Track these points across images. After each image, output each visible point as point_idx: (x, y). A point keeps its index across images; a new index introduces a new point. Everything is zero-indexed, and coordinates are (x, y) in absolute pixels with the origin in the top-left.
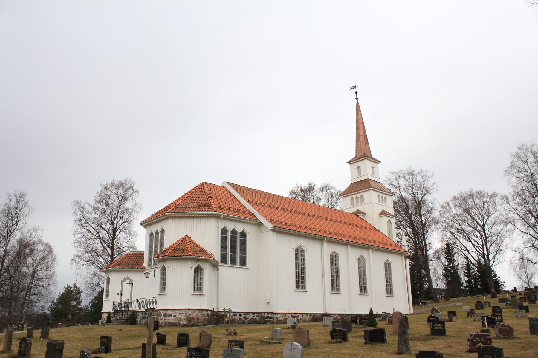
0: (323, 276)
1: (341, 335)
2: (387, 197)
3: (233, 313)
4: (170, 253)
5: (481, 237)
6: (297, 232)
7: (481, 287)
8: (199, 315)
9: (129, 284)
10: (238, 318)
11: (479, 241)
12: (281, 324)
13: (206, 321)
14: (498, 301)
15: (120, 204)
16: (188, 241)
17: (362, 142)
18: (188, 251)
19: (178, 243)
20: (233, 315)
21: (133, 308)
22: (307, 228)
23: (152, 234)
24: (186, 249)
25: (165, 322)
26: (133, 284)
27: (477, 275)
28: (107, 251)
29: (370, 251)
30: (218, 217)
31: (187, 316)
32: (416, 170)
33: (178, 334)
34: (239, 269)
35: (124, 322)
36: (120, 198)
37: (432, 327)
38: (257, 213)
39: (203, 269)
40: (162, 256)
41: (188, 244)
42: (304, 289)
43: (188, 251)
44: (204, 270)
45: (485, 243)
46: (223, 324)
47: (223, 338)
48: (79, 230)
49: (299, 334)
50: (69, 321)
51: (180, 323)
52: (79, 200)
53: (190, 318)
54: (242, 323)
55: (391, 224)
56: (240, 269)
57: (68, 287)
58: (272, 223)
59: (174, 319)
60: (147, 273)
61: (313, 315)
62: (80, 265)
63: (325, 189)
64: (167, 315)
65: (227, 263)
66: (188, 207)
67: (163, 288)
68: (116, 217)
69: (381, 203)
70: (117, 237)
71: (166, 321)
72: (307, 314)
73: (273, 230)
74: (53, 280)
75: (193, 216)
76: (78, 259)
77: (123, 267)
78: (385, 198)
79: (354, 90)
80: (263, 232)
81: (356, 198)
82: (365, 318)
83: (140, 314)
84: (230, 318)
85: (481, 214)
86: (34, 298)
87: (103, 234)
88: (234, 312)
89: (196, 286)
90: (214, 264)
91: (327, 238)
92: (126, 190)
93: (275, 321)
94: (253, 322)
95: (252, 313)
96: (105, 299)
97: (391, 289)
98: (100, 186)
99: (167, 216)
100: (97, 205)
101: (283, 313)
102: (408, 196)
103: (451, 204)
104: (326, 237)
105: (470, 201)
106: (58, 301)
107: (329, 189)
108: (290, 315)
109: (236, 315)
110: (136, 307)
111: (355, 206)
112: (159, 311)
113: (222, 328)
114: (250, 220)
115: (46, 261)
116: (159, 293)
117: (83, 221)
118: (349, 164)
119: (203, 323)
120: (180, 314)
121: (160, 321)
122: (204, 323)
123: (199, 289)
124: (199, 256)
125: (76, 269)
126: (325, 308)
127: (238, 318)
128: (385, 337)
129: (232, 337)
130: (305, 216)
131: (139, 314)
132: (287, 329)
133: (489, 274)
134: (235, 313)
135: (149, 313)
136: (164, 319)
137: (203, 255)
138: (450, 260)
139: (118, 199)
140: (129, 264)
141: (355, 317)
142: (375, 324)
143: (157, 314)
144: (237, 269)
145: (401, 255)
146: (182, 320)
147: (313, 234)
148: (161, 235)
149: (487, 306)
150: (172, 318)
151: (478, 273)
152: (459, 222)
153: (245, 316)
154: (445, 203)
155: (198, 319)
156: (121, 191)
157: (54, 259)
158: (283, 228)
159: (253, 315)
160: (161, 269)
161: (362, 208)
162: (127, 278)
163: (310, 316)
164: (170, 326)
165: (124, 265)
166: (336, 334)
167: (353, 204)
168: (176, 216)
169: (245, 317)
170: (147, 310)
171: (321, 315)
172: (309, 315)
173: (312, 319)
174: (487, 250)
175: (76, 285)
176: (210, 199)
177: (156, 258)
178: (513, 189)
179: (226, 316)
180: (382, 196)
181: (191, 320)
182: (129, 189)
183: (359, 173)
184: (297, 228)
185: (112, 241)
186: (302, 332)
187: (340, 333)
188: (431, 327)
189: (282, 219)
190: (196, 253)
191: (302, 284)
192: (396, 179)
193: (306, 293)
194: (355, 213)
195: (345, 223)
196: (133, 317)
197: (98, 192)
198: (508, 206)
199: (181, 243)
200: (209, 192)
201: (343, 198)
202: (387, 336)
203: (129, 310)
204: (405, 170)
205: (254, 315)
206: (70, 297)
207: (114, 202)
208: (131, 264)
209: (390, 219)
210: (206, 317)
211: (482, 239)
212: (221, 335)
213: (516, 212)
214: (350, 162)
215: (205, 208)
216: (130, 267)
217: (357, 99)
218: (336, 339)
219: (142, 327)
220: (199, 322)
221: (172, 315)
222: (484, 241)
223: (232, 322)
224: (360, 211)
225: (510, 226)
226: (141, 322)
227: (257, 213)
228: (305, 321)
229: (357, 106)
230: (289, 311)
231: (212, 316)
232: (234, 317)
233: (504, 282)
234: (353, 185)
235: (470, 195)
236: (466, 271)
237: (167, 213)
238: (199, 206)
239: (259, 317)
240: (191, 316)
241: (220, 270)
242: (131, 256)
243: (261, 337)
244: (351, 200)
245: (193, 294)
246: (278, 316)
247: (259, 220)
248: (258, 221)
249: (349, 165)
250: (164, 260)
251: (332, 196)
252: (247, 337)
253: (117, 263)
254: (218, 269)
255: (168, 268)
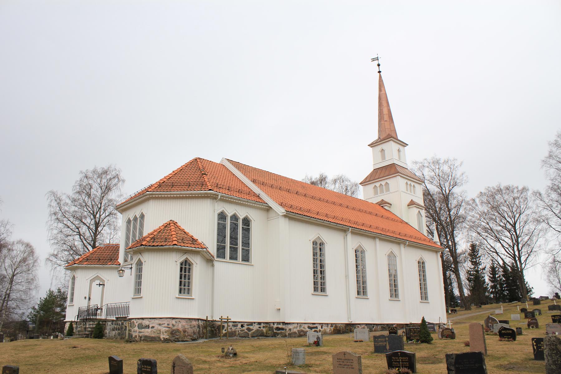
0: (347, 276)
1: (406, 362)
2: (416, 185)
3: (232, 323)
4: (148, 242)
5: (512, 237)
6: (316, 220)
7: (507, 293)
8: (186, 327)
9: (100, 285)
10: (240, 329)
11: (510, 242)
12: (295, 337)
13: (196, 335)
14: (548, 309)
15: (103, 195)
16: (172, 227)
17: (386, 121)
18: (172, 239)
19: (160, 230)
20: (233, 326)
21: (102, 316)
22: (326, 215)
23: (129, 222)
24: (170, 236)
25: (139, 336)
26: (104, 285)
27: (502, 280)
28: (88, 249)
29: (402, 246)
30: (214, 198)
31: (169, 328)
32: (442, 157)
33: (140, 360)
34: (240, 265)
35: (88, 335)
36: (104, 188)
37: (535, 347)
38: (264, 195)
39: (193, 264)
40: (137, 247)
41: (173, 230)
42: (324, 292)
43: (172, 239)
44: (194, 265)
45: (516, 244)
46: (219, 338)
47: (217, 363)
48: (56, 225)
49: (344, 364)
50: (29, 331)
51: (159, 338)
52: (55, 190)
53: (173, 331)
54: (245, 336)
55: (422, 216)
56: (242, 265)
57: (51, 293)
58: (284, 207)
59: (151, 331)
60: (121, 270)
61: (335, 325)
62: (56, 266)
63: (339, 181)
64: (143, 325)
65: (225, 258)
66: (176, 186)
67: (138, 290)
68: (99, 210)
69: (409, 192)
70: (100, 234)
71: (141, 334)
72: (328, 324)
73: (285, 216)
74: (35, 284)
75: (181, 196)
76: (54, 260)
77: (92, 263)
78: (414, 186)
79: (376, 62)
80: (272, 219)
81: (379, 186)
82: (414, 331)
83: (110, 323)
84: (229, 330)
85: (512, 212)
86: (12, 304)
87: (84, 229)
88: (234, 322)
89: (182, 287)
90: (208, 259)
91: (352, 228)
92: (110, 179)
93: (287, 334)
94: (260, 335)
95: (257, 323)
96: (70, 304)
97: (426, 293)
98: (79, 173)
99: (148, 196)
100: (77, 196)
101: (297, 323)
102: (433, 189)
103: (477, 201)
104: (351, 227)
105: (498, 197)
106: (40, 307)
107: (343, 181)
108: (306, 326)
109: (237, 326)
110: (105, 316)
111: (379, 196)
112: (132, 321)
113: (216, 344)
114: (255, 204)
115: (27, 263)
116: (133, 296)
117: (59, 216)
118: (371, 147)
119: (191, 337)
120: (160, 325)
121: (134, 334)
122: (193, 337)
123: (186, 291)
124: (188, 247)
125: (52, 270)
126: (349, 317)
127: (240, 329)
128: (484, 367)
129: (230, 360)
130: (323, 203)
131: (109, 324)
132: (307, 346)
133: (521, 279)
134: (235, 324)
135: (120, 323)
136: (138, 332)
137: (193, 246)
138: (476, 264)
139: (102, 189)
140: (100, 260)
141: (394, 329)
142: (430, 340)
143: (129, 324)
144: (238, 265)
145: (436, 252)
146: (163, 333)
147: (335, 223)
148: (140, 221)
149: (537, 315)
150: (150, 330)
151: (504, 279)
152: (487, 221)
153: (249, 327)
154: (471, 200)
155: (185, 331)
156: (104, 181)
157: (35, 261)
158: (298, 214)
159: (259, 326)
160: (136, 264)
161: (387, 198)
162: (97, 278)
163: (332, 326)
164: (146, 340)
165: (94, 261)
166: (395, 359)
167: (376, 193)
168: (160, 196)
169: (249, 328)
170: (119, 319)
171: (344, 325)
172: (330, 325)
173: (334, 331)
174: (519, 251)
175: (60, 290)
176: (204, 176)
177: (129, 249)
178: (550, 182)
179: (223, 327)
180: (410, 185)
181: (175, 333)
182: (114, 178)
183: (383, 157)
184: (315, 215)
185: (93, 238)
186: (349, 360)
187: (404, 358)
188: (534, 348)
189: (295, 204)
190: (183, 243)
191: (321, 285)
192: (419, 169)
193: (326, 297)
194: (379, 204)
195: (370, 213)
196: (99, 329)
197: (78, 181)
198: (541, 202)
199: (164, 229)
200: (203, 168)
201: (364, 186)
202: (487, 365)
203: (97, 318)
204: (429, 158)
205: (260, 326)
206: (53, 303)
207: (96, 192)
208: (102, 260)
209: (421, 211)
210: (196, 330)
211: (512, 239)
212: (213, 357)
213: (551, 210)
214: (372, 145)
215: (197, 186)
216: (101, 263)
217: (379, 72)
218: (397, 369)
219: (108, 341)
220: (187, 335)
221: (149, 325)
222: (514, 241)
223: (232, 334)
224: (385, 201)
225: (544, 225)
226: (111, 335)
227: (264, 195)
228: (325, 333)
229: (380, 80)
230: (305, 320)
231: (205, 327)
232: (234, 329)
233: (532, 288)
234: (376, 170)
235: (498, 191)
236: (491, 276)
237: (147, 192)
238: (189, 183)
239: (267, 329)
240: (175, 328)
241: (215, 267)
242: (103, 250)
243: (274, 362)
244: (374, 188)
245: (178, 298)
246: (290, 327)
247: (267, 203)
248: (266, 205)
249: (371, 148)
250: (140, 252)
251: (347, 189)
252: (253, 360)
253: (85, 258)
254: (213, 266)
255: (145, 262)
